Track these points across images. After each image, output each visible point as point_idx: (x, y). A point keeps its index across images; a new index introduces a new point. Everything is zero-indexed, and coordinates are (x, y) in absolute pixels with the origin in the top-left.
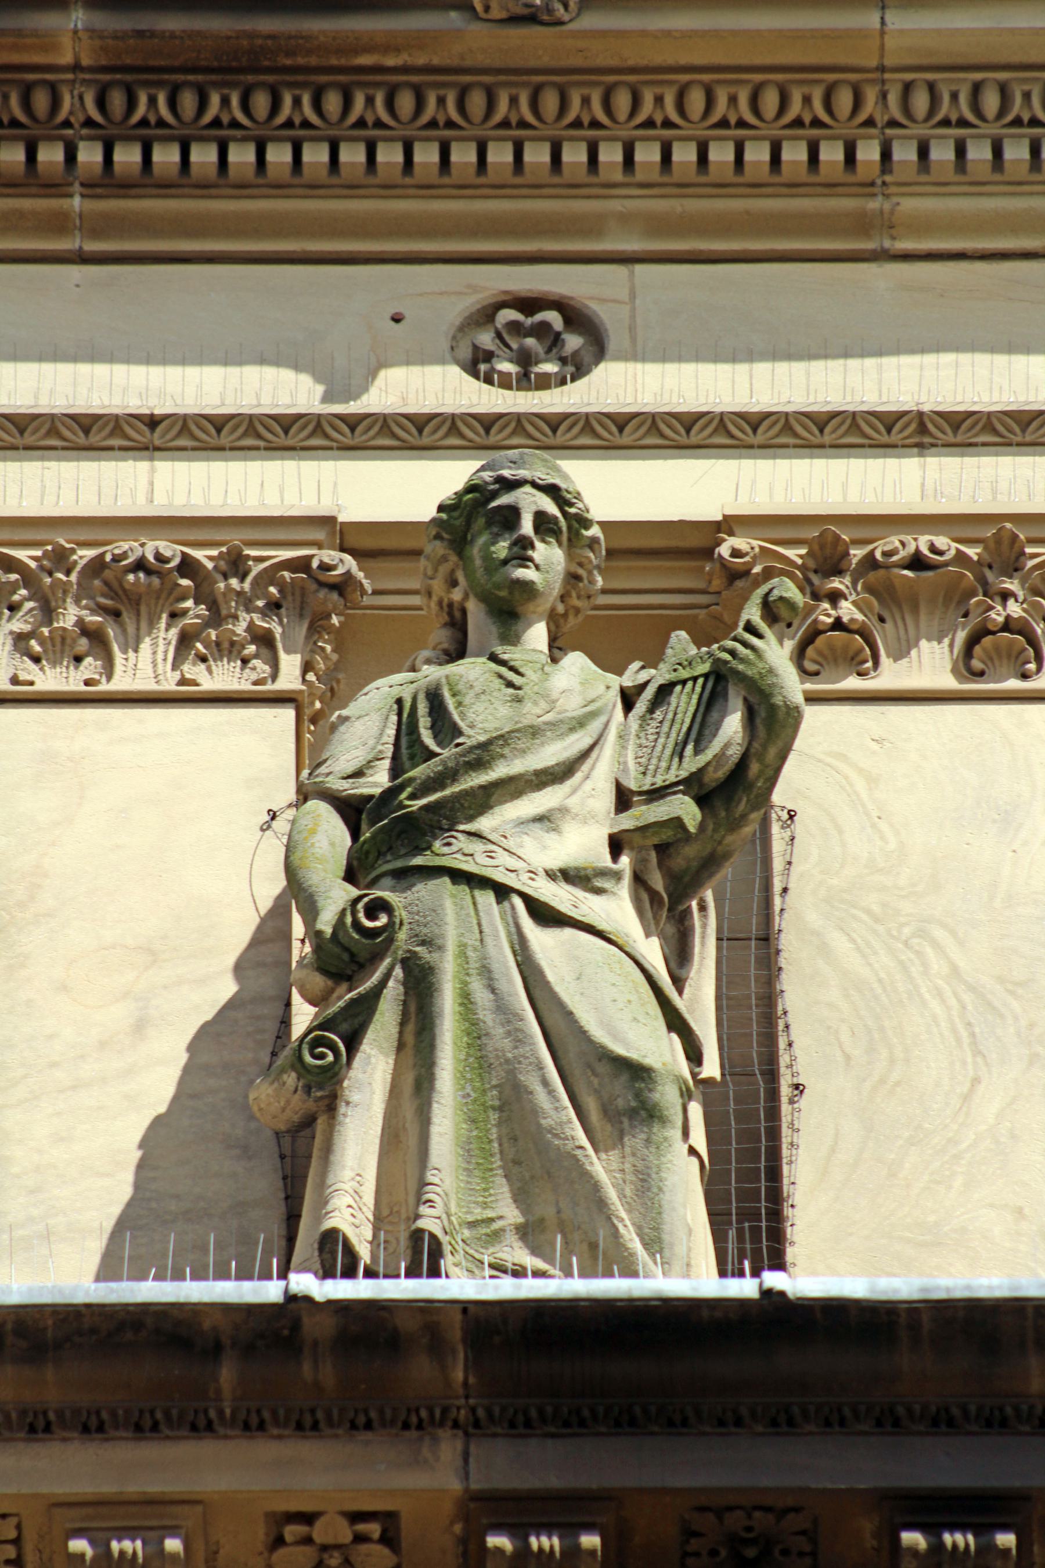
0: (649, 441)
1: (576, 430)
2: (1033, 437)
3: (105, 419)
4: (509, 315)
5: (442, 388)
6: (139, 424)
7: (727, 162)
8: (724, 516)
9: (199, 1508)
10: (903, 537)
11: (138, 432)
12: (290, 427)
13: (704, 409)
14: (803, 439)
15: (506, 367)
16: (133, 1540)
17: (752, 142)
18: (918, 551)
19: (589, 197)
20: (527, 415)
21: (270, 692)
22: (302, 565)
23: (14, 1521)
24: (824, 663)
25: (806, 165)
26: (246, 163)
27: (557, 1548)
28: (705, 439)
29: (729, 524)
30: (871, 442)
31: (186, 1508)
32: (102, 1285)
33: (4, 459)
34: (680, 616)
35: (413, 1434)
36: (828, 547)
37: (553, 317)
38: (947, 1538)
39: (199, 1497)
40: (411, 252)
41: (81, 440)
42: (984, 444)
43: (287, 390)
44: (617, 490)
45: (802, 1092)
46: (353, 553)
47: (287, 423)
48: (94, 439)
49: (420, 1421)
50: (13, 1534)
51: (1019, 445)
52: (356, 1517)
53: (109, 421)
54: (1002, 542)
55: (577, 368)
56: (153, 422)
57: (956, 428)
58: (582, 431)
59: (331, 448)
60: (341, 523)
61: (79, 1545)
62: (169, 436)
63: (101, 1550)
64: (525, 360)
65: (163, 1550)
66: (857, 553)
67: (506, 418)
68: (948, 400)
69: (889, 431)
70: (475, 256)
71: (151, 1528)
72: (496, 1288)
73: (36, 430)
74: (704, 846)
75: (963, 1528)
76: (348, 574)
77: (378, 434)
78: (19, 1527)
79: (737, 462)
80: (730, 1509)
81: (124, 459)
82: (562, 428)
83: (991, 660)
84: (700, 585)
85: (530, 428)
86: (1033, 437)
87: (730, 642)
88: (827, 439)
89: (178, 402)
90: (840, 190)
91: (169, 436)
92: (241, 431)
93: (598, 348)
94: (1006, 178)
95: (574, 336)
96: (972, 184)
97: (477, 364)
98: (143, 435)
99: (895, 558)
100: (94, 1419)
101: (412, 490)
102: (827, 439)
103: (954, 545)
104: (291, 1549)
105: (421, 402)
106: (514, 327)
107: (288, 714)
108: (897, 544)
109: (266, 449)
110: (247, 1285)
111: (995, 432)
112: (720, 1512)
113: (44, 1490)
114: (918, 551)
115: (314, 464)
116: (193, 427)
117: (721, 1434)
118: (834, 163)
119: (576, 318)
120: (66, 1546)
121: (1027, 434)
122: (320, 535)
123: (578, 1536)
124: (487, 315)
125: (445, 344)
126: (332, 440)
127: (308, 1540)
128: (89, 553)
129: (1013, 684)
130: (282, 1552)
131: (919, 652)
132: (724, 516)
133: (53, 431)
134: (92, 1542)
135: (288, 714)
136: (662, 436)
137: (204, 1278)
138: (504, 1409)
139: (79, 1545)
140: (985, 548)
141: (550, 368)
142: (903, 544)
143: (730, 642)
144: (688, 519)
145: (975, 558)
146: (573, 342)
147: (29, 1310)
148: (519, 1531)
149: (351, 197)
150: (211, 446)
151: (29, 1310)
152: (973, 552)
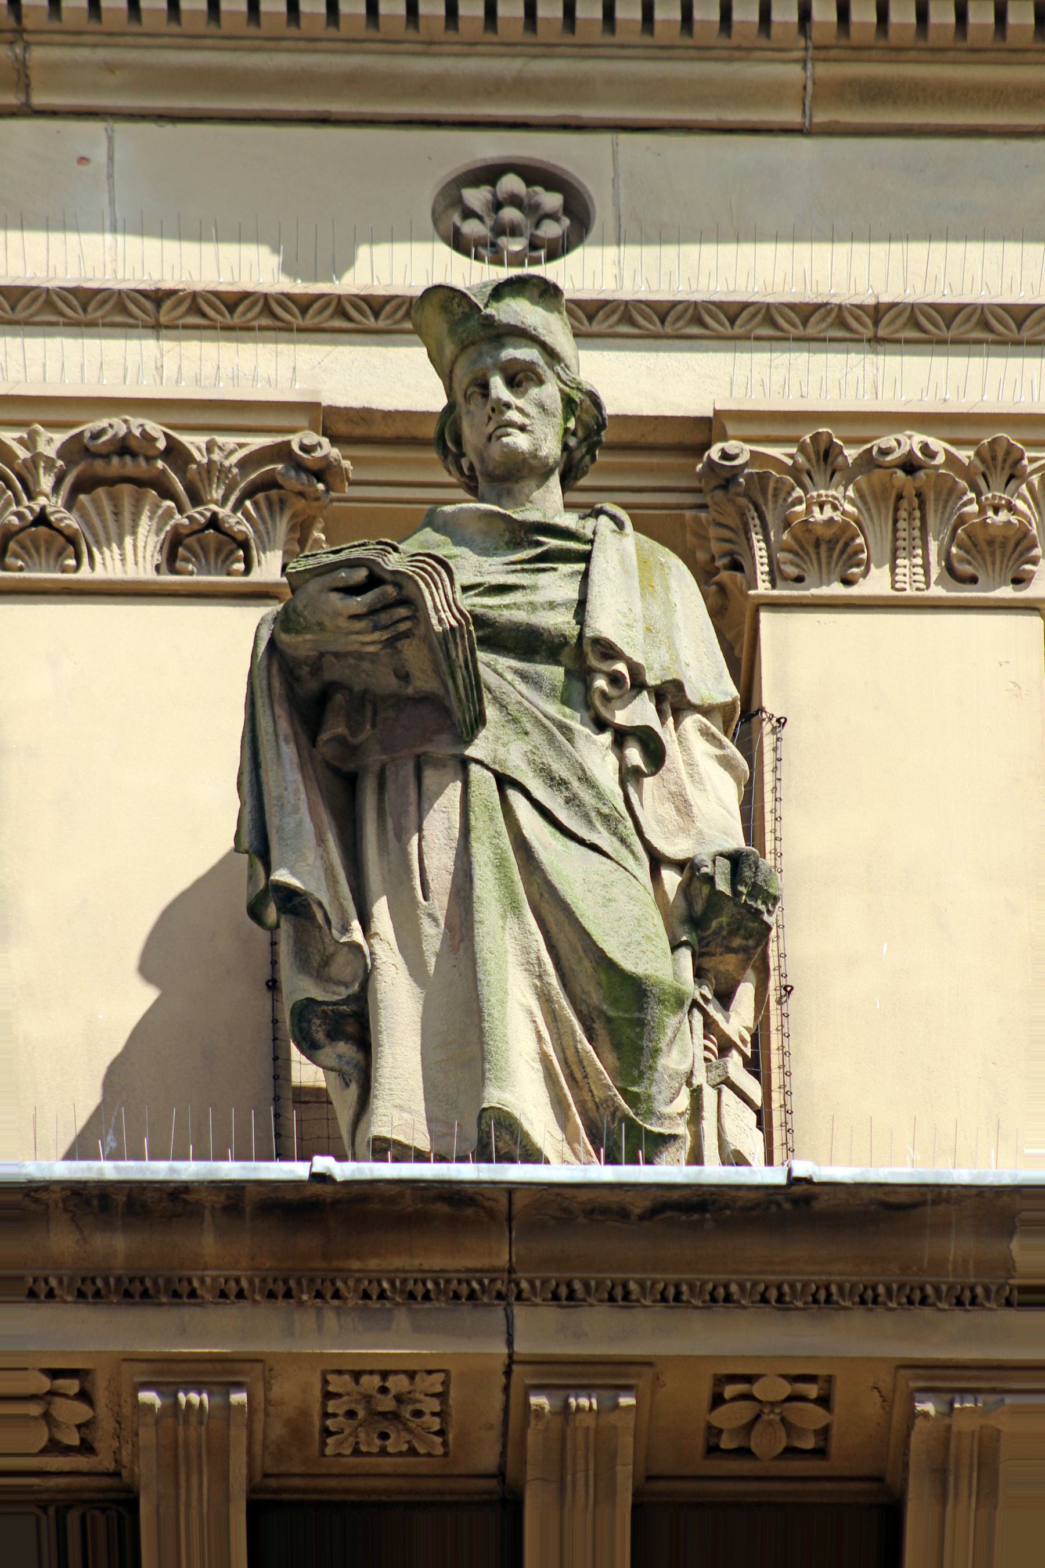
1: (108, 307)
3: (680, 307)
5: (411, 265)
7: (633, 21)
8: (716, 412)
9: (259, 1366)
10: (900, 437)
16: (589, 1398)
18: (911, 452)
20: (991, 306)
21: (814, 596)
22: (282, 452)
23: (441, 1376)
25: (757, 25)
26: (748, 23)
27: (595, 1406)
30: (646, 332)
31: (247, 1366)
32: (68, 1163)
33: (4, 334)
35: (281, 1303)
36: (822, 445)
38: (972, 1405)
39: (259, 1358)
41: (657, 328)
42: (832, 340)
43: (253, 267)
44: (636, 383)
45: (789, 992)
46: (335, 440)
47: (233, 301)
48: (93, 315)
49: (428, 1292)
50: (439, 1389)
51: (300, 330)
52: (55, 1374)
53: (110, 296)
54: (997, 449)
57: (231, 308)
58: (260, 314)
59: (135, 326)
61: (148, 1397)
63: (170, 1401)
65: (229, 1403)
66: (851, 453)
67: (103, 293)
68: (39, 275)
69: (663, 321)
70: (355, 117)
71: (167, 1384)
72: (479, 1171)
75: (199, 1388)
77: (831, 325)
78: (445, 1383)
79: (1004, 360)
80: (396, 1372)
83: (983, 565)
86: (316, 321)
88: (1025, 335)
89: (654, 288)
90: (285, 44)
91: (250, 315)
92: (615, 318)
94: (1006, 45)
96: (267, 39)
97: (459, 243)
99: (889, 458)
100: (967, 1294)
102: (1025, 335)
103: (748, 447)
104: (730, 1405)
105: (712, 288)
108: (895, 444)
109: (65, 324)
110: (179, 1165)
111: (775, 325)
112: (357, 1375)
113: (111, 1348)
114: (911, 452)
115: (96, 342)
117: (176, 1304)
120: (136, 1397)
121: (735, 327)
122: (303, 421)
123: (617, 1396)
126: (136, 318)
127: (748, 1397)
129: (836, 589)
130: (724, 1408)
132: (716, 412)
134: (160, 1394)
137: (248, 1158)
138: (544, 1282)
139: (148, 1397)
140: (978, 454)
142: (899, 443)
144: (630, 413)
145: (966, 462)
147: (741, 1193)
148: (167, 1389)
151: (741, 1193)
152: (965, 455)
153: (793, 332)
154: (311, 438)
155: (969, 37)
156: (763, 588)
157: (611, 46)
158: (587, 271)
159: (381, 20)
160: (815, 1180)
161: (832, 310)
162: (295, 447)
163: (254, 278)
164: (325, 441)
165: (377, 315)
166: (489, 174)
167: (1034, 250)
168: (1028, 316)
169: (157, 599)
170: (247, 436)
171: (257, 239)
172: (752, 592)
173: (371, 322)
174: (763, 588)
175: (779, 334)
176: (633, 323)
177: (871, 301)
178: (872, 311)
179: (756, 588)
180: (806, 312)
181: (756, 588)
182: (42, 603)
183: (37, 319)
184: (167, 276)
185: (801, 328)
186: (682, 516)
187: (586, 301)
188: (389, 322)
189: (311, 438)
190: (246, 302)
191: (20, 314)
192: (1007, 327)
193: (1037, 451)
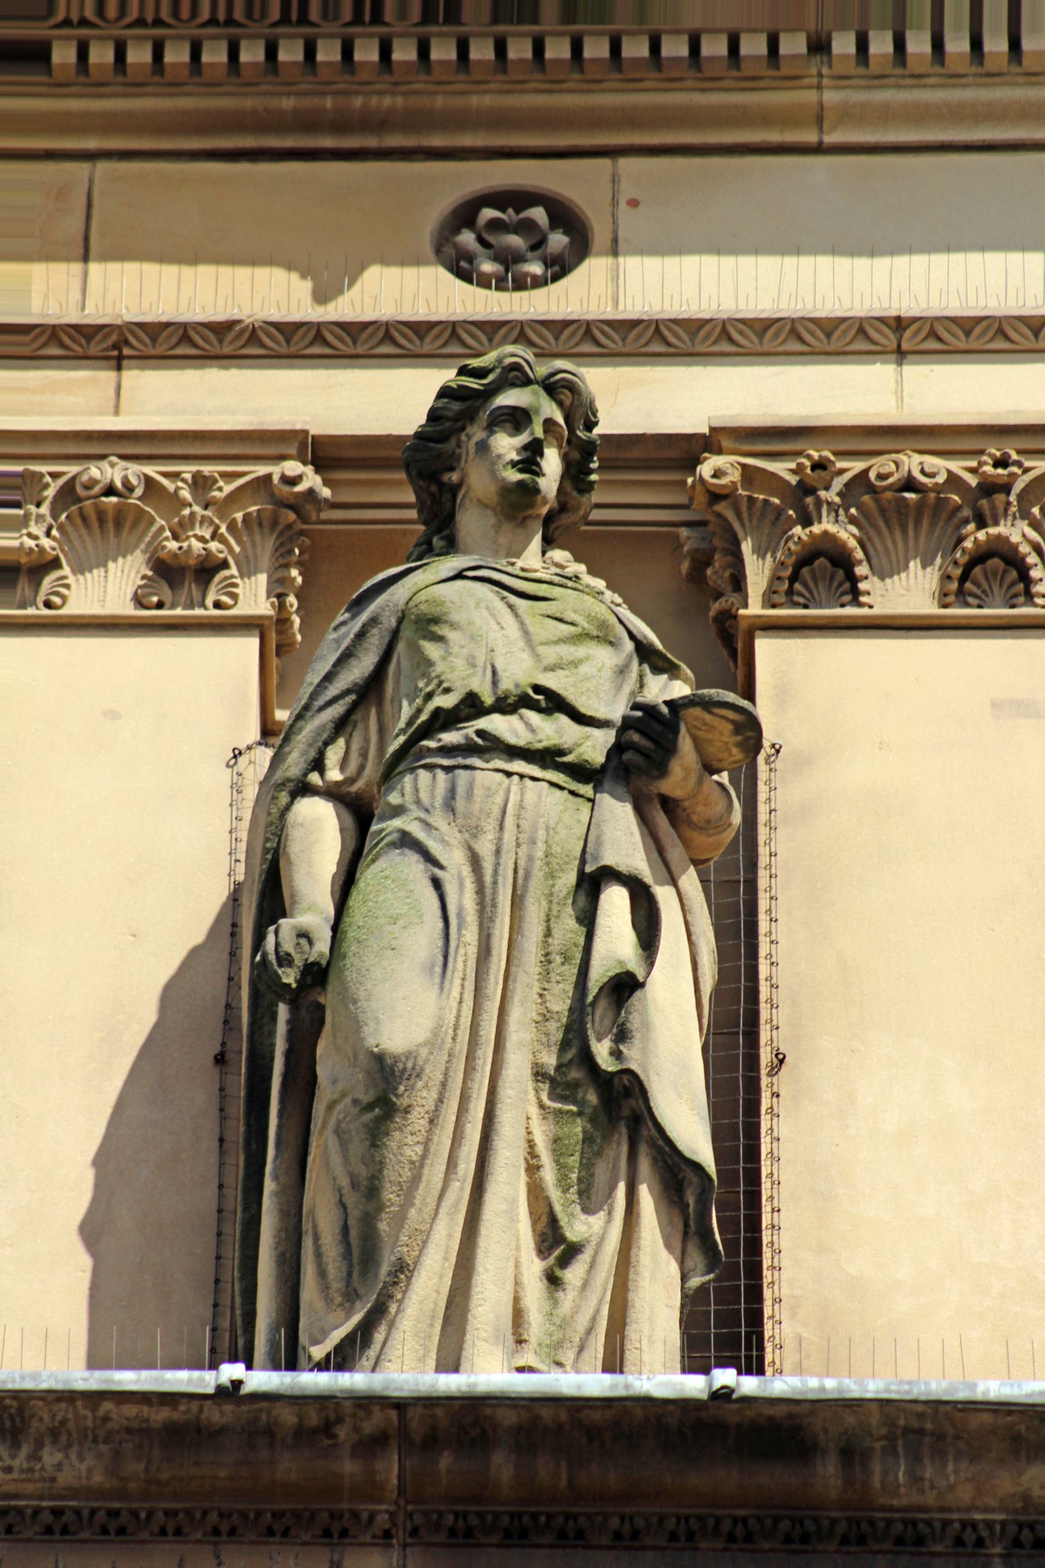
0: (856, 346)
2: (840, 344)
4: (488, 213)
6: (747, 331)
11: (953, 335)
12: (159, 335)
13: (707, 316)
14: (809, 345)
15: (488, 267)
17: (787, 34)
19: (643, 90)
24: (155, 585)
28: (236, 350)
29: (710, 442)
34: (595, 531)
37: (538, 214)
40: (607, 146)
43: (273, 294)
47: (288, 330)
55: (560, 268)
56: (899, 324)
60: (313, 437)
62: (572, 343)
64: (509, 259)
73: (983, 333)
74: (681, 769)
76: (311, 491)
81: (874, 363)
82: (838, 333)
84: (683, 499)
85: (465, 336)
87: (725, 557)
90: (853, 82)
93: (581, 247)
95: (568, 238)
97: (463, 269)
98: (1023, 338)
101: (396, 400)
106: (495, 225)
107: (251, 644)
116: (396, 335)
118: (921, 55)
119: (564, 217)
124: (465, 215)
125: (428, 249)
128: (857, 466)
131: (106, 572)
132: (712, 429)
133: (1001, 333)
135: (251, 644)
136: (598, 344)
141: (536, 268)
143: (725, 557)
146: (558, 241)
149: (712, 90)
150: (818, 350)
153: (1026, 345)
154: (292, 467)
155: (871, 66)
156: (754, 608)
157: (776, 78)
158: (585, 293)
159: (909, 59)
160: (585, 1277)
161: (717, 325)
162: (276, 479)
163: (982, 303)
164: (309, 470)
165: (421, 338)
166: (499, 199)
167: (1035, 260)
168: (836, 327)
169: (824, 632)
170: (1035, 459)
171: (362, 268)
172: (741, 612)
173: (415, 347)
174: (754, 608)
175: (805, 348)
176: (326, 343)
177: (893, 313)
178: (894, 324)
179: (746, 606)
180: (967, 325)
181: (746, 606)
182: (814, 637)
183: (308, 351)
184: (857, 305)
185: (151, 347)
186: (677, 536)
187: (962, 318)
188: (430, 347)
189: (292, 467)
190: (843, 326)
191: (835, 345)
192: (277, 342)
193: (235, 465)
